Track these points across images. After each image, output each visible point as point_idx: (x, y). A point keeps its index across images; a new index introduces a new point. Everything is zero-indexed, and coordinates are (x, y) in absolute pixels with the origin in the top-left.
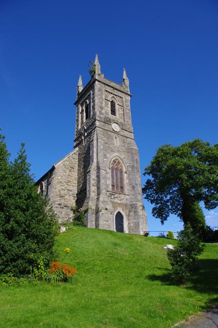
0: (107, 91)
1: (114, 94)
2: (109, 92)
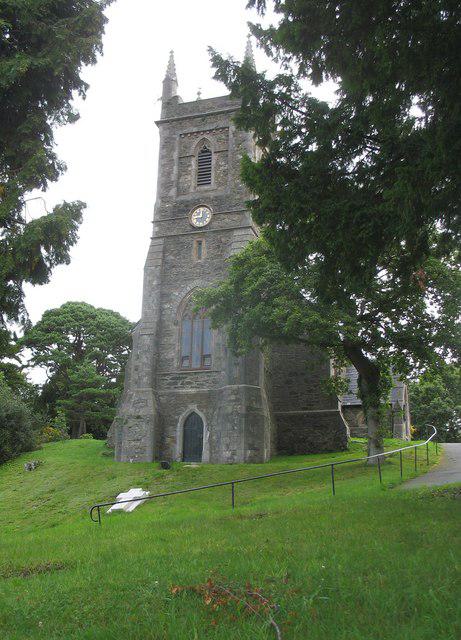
0: (186, 134)
1: (198, 132)
2: (192, 134)
